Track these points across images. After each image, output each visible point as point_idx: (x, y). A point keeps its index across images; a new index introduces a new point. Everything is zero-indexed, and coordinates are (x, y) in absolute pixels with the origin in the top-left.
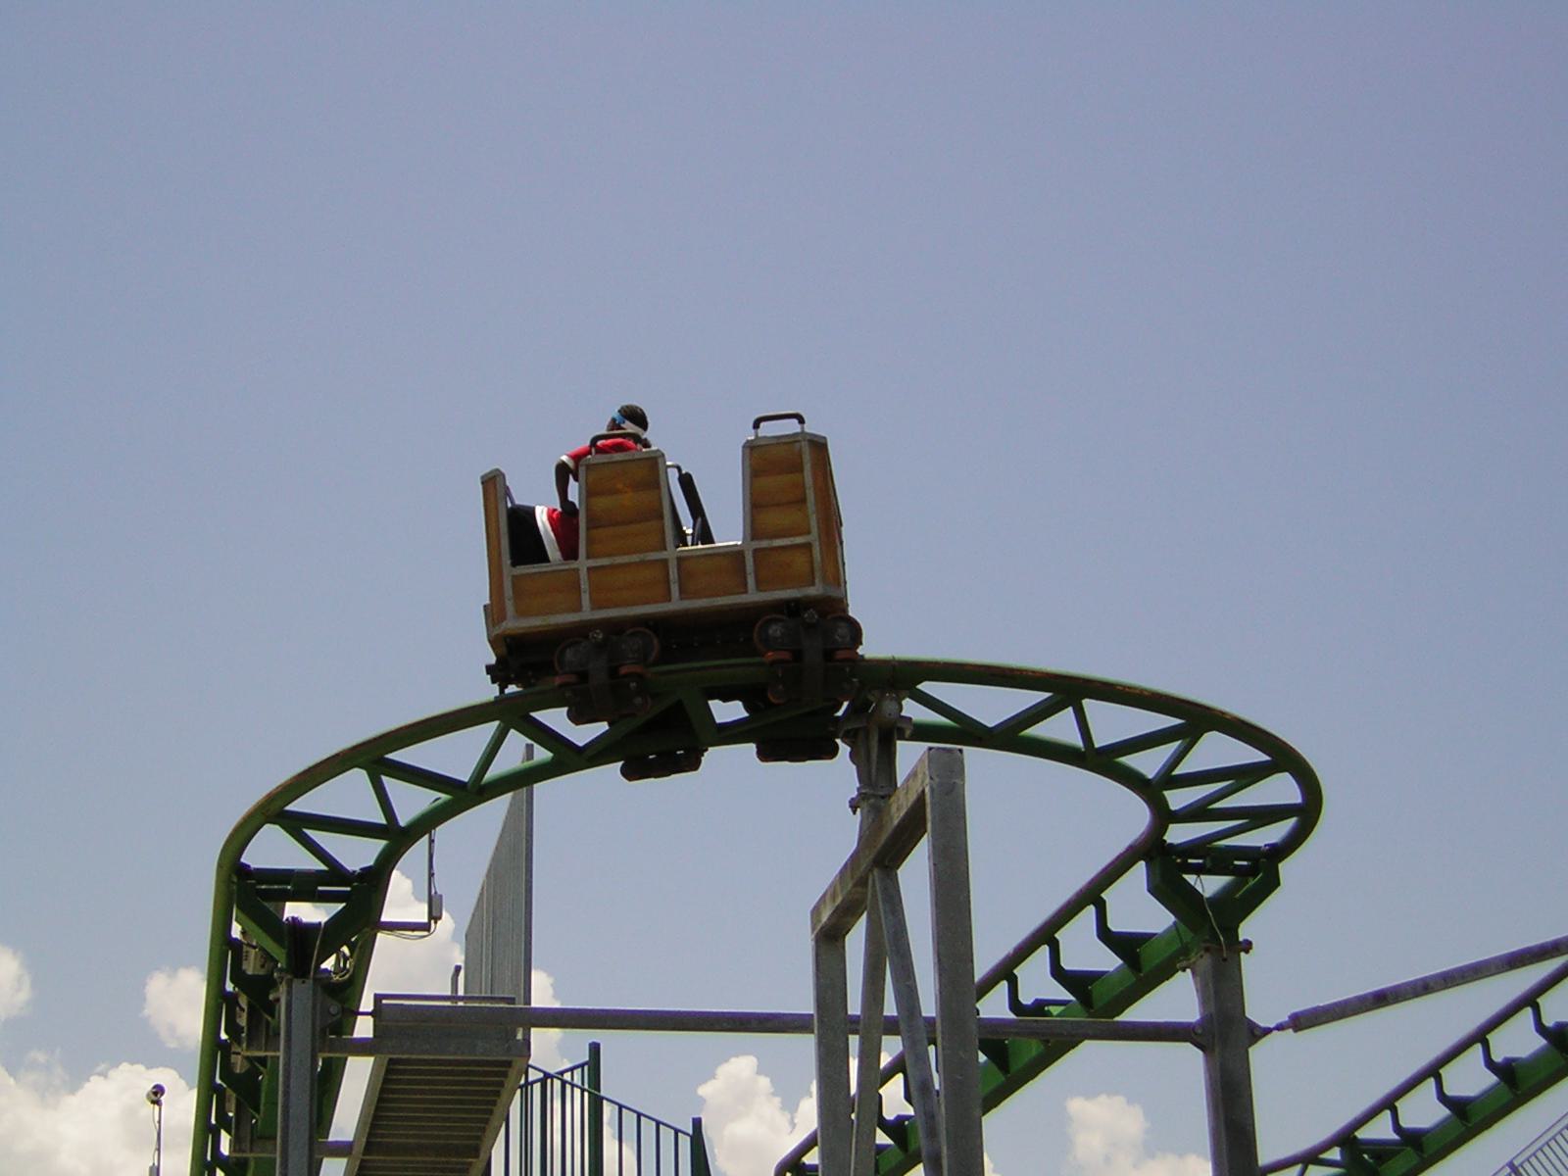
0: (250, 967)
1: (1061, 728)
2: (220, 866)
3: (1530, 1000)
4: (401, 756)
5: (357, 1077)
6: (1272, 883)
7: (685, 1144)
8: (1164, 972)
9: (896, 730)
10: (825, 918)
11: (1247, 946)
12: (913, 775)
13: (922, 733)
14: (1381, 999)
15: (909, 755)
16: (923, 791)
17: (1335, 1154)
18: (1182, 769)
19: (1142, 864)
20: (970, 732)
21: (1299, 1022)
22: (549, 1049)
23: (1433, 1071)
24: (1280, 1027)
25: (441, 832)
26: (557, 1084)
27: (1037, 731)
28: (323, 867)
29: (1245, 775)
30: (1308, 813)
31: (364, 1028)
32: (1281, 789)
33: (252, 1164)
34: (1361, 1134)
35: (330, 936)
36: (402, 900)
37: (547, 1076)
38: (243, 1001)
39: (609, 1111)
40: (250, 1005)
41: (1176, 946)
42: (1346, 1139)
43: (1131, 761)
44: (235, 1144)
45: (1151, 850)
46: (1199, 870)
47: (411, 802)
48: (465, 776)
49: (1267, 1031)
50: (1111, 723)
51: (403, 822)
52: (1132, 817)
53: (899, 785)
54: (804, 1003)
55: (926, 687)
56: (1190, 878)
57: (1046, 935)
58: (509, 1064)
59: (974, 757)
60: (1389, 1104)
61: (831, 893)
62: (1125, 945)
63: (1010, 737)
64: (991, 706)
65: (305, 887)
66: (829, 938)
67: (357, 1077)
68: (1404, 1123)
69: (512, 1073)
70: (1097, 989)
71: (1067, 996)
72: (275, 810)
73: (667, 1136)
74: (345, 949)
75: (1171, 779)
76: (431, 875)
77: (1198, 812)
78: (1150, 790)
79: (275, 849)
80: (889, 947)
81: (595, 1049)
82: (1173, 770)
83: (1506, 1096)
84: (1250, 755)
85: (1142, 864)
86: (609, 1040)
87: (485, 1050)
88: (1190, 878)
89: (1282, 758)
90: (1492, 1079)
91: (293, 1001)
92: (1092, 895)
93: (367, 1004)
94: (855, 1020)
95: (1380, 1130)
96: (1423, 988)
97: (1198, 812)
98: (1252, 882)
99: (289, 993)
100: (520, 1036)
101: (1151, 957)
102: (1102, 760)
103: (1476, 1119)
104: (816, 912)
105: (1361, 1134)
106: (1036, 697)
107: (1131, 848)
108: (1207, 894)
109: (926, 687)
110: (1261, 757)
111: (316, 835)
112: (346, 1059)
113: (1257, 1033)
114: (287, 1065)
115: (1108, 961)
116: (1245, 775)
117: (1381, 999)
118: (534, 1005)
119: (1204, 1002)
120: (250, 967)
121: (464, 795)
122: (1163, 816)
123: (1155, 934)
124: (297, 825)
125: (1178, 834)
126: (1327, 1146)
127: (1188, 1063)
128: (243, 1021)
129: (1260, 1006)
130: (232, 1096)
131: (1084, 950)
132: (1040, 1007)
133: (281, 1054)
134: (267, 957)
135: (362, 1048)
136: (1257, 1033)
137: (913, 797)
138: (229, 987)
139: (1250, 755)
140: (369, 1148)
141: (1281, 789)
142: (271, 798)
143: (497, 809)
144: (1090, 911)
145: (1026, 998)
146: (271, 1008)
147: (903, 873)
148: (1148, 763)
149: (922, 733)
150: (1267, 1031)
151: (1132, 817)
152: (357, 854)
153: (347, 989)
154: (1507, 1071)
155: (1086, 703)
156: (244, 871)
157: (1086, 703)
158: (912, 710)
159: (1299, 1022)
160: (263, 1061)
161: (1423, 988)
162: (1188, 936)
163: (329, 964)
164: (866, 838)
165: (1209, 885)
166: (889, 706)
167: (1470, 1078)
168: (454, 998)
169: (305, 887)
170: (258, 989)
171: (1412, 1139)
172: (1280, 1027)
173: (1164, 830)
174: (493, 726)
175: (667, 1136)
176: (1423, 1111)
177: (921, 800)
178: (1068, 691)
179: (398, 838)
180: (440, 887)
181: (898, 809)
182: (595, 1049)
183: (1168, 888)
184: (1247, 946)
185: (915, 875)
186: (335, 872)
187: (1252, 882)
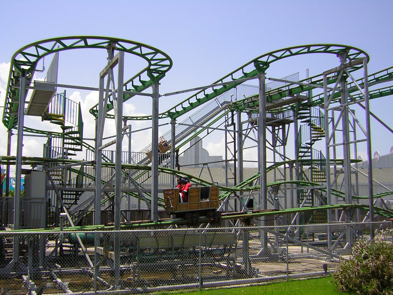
0: (15, 75)
1: (138, 51)
2: (12, 59)
3: (196, 95)
4: (40, 45)
5: (31, 92)
6: (164, 75)
7: (78, 105)
8: (148, 87)
9: (114, 49)
10: (102, 75)
11: (160, 84)
12: (117, 55)
13: (118, 49)
14: (177, 93)
15: (116, 52)
16: (118, 58)
17: (167, 114)
18: (154, 58)
19: (146, 71)
20: (124, 50)
21: (166, 95)
22: (60, 90)
23: (181, 103)
24: (163, 95)
25: (45, 57)
26: (59, 95)
27: (134, 51)
28: (27, 61)
29: (163, 60)
30: (170, 66)
31: (32, 85)
32: (167, 62)
33: (14, 104)
34: (171, 111)
35: (29, 71)
36: (39, 66)
37: (58, 94)
38: (14, 80)
39: (67, 100)
40: (15, 81)
41: (150, 83)
42: (169, 112)
43: (147, 56)
44: (12, 101)
45: (148, 69)
46: (154, 73)
47: (41, 52)
48: (50, 49)
49: (161, 96)
50: (145, 51)
51: (40, 55)
52: (146, 64)
53: (114, 56)
54: (98, 87)
55: (119, 43)
56: (153, 74)
57: (132, 80)
58: (53, 92)
59: (126, 53)
60: (175, 107)
61: (103, 71)
62: (143, 82)
63: (130, 51)
64: (128, 46)
65: (24, 63)
66: (102, 77)
67: (31, 92)
68: (177, 110)
69: (54, 93)
70: (138, 88)
71: (134, 89)
72: (21, 52)
73: (75, 104)
74: (30, 73)
75: (152, 59)
76: (44, 63)
77: (155, 65)
78: (149, 61)
79: (20, 58)
80: (111, 79)
81: (65, 91)
82: (165, 59)
83: (191, 107)
84: (164, 57)
85: (146, 71)
86: (67, 89)
87: (50, 90)
88: (153, 74)
89: (168, 58)
90: (182, 109)
91: (22, 80)
92: (139, 75)
93: (33, 81)
94: (105, 89)
95: (173, 111)
96: (183, 92)
97: (155, 65)
98: (161, 75)
99: (22, 79)
100: (55, 88)
101: (146, 84)
102: (143, 56)
103: (194, 106)
104: (100, 74)
105: (171, 111)
106: (135, 46)
107: (145, 69)
108: (155, 76)
109: (119, 43)
110: (165, 58)
111: (26, 56)
112: (28, 90)
113: (160, 96)
114: (21, 89)
115: (140, 84)
116: (163, 60)
117: (177, 93)
118: (58, 83)
119: (153, 91)
120: (15, 75)
121: (50, 52)
122: (150, 65)
123: (146, 81)
124: (24, 54)
125: (152, 67)
126: (166, 112)
127: (150, 99)
128: (14, 83)
129: (161, 92)
130: (12, 94)
131: (137, 82)
132: (130, 90)
133: (20, 88)
134: (18, 73)
135: (32, 88)
136: (160, 96)
137: (117, 58)
138: (12, 77)
139: (164, 57)
140: (32, 103)
141: (167, 62)
142: (21, 50)
143: (54, 54)
144: (138, 77)
145: (128, 89)
146: (18, 81)
147: (114, 69)
148: (149, 57)
149: (118, 49)
150: (161, 96)
151: (146, 64)
152: (32, 59)
153: (29, 79)
154: (191, 104)
155: (142, 47)
156: (15, 60)
157: (142, 47)
158: (117, 46)
159: (166, 95)
160: (17, 89)
161: (183, 92)
162: (152, 82)
163: (28, 75)
164: (109, 64)
165: (156, 75)
166: (114, 45)
167: (186, 105)
168: (45, 82)
169: (24, 63)
170: (17, 78)
171: (178, 112)
172: (163, 95)
173: (150, 66)
174: (55, 42)
175: (75, 104)
176: (179, 109)
177: (118, 58)
178: (140, 45)
179: (39, 57)
180: (45, 66)
181: (114, 60)
182: (65, 91)
183: (150, 75)
184: (160, 84)
185: (116, 69)
186: (29, 62)
187: (161, 75)
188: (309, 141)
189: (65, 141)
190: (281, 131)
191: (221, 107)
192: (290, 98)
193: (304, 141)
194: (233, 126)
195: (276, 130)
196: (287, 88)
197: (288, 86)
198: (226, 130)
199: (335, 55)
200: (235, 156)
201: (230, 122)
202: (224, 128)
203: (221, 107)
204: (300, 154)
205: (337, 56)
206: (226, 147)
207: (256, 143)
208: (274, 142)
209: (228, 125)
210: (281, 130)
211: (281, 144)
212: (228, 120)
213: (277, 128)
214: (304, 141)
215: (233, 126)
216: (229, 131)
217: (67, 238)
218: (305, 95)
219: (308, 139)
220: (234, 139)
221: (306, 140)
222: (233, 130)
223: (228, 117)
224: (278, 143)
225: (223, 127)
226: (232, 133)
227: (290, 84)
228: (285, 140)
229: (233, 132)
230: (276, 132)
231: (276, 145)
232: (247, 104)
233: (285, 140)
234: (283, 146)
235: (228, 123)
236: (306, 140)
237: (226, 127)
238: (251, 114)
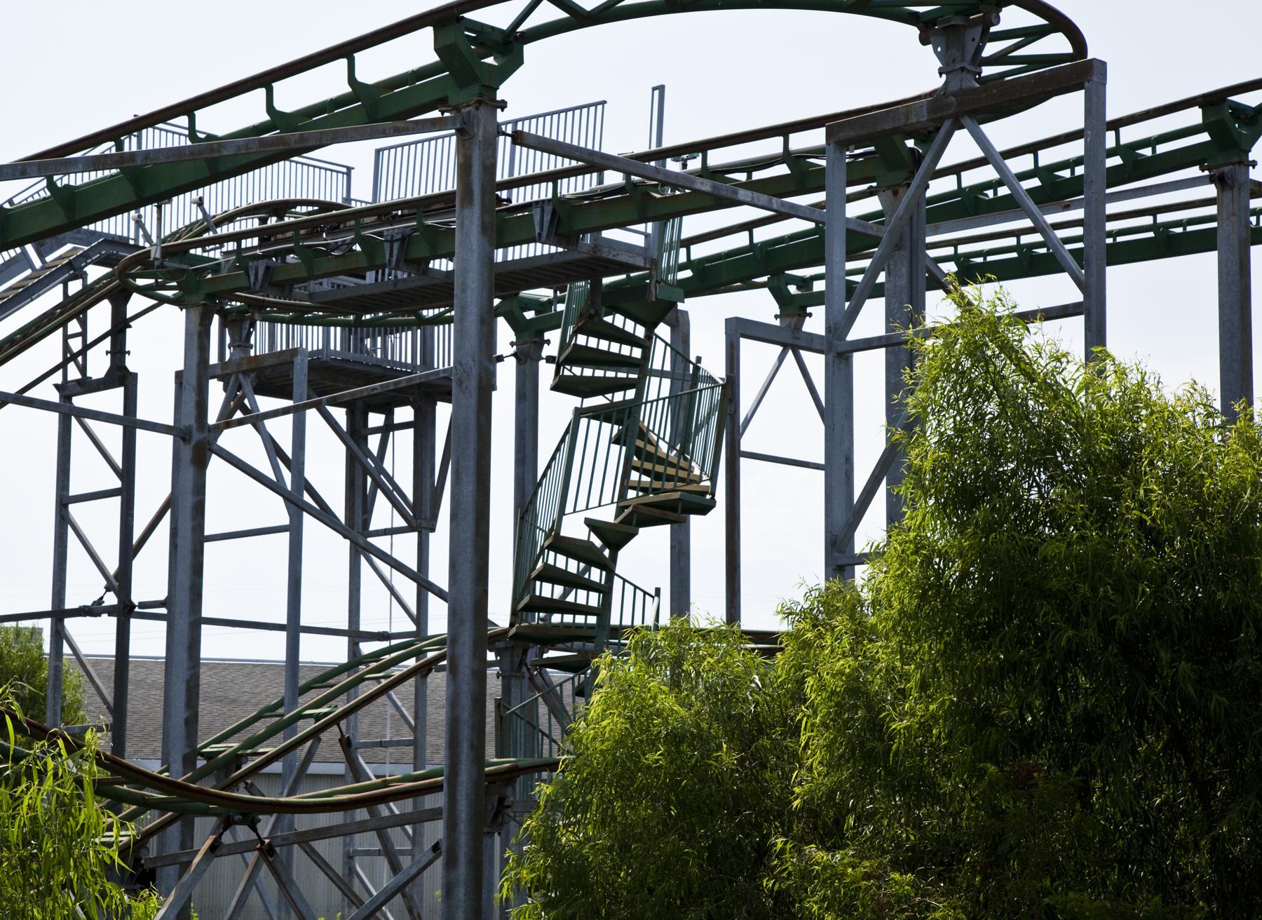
29: (1032, 34)
116: (1032, 34)
139: (1036, 20)
188: (608, 515)
189: (667, 400)
190: (404, 442)
191: (38, 264)
192: (553, 249)
193: (581, 505)
194: (119, 392)
195: (375, 431)
196: (543, 192)
197: (553, 177)
198: (67, 413)
199: (914, 32)
200: (121, 581)
201: (99, 363)
202: (55, 397)
203: (38, 264)
204: (546, 590)
205: (924, 41)
206: (63, 521)
207: (279, 500)
208: (359, 501)
209: (87, 386)
210: (410, 433)
211: (400, 522)
212: (83, 352)
213: (376, 420)
214: (581, 505)
215: (119, 392)
216: (83, 414)
217: (1229, 831)
218: (639, 241)
219: (607, 498)
220: (127, 472)
221: (594, 501)
222: (120, 412)
223: (83, 334)
224: (383, 514)
225: (48, 391)
226: (112, 436)
227: (568, 163)
228: (427, 496)
229: (118, 430)
230: (374, 442)
231: (367, 522)
232: (262, 265)
233: (427, 496)
234: (415, 535)
235: (83, 369)
236: (594, 501)
237: (66, 390)
238: (253, 325)
